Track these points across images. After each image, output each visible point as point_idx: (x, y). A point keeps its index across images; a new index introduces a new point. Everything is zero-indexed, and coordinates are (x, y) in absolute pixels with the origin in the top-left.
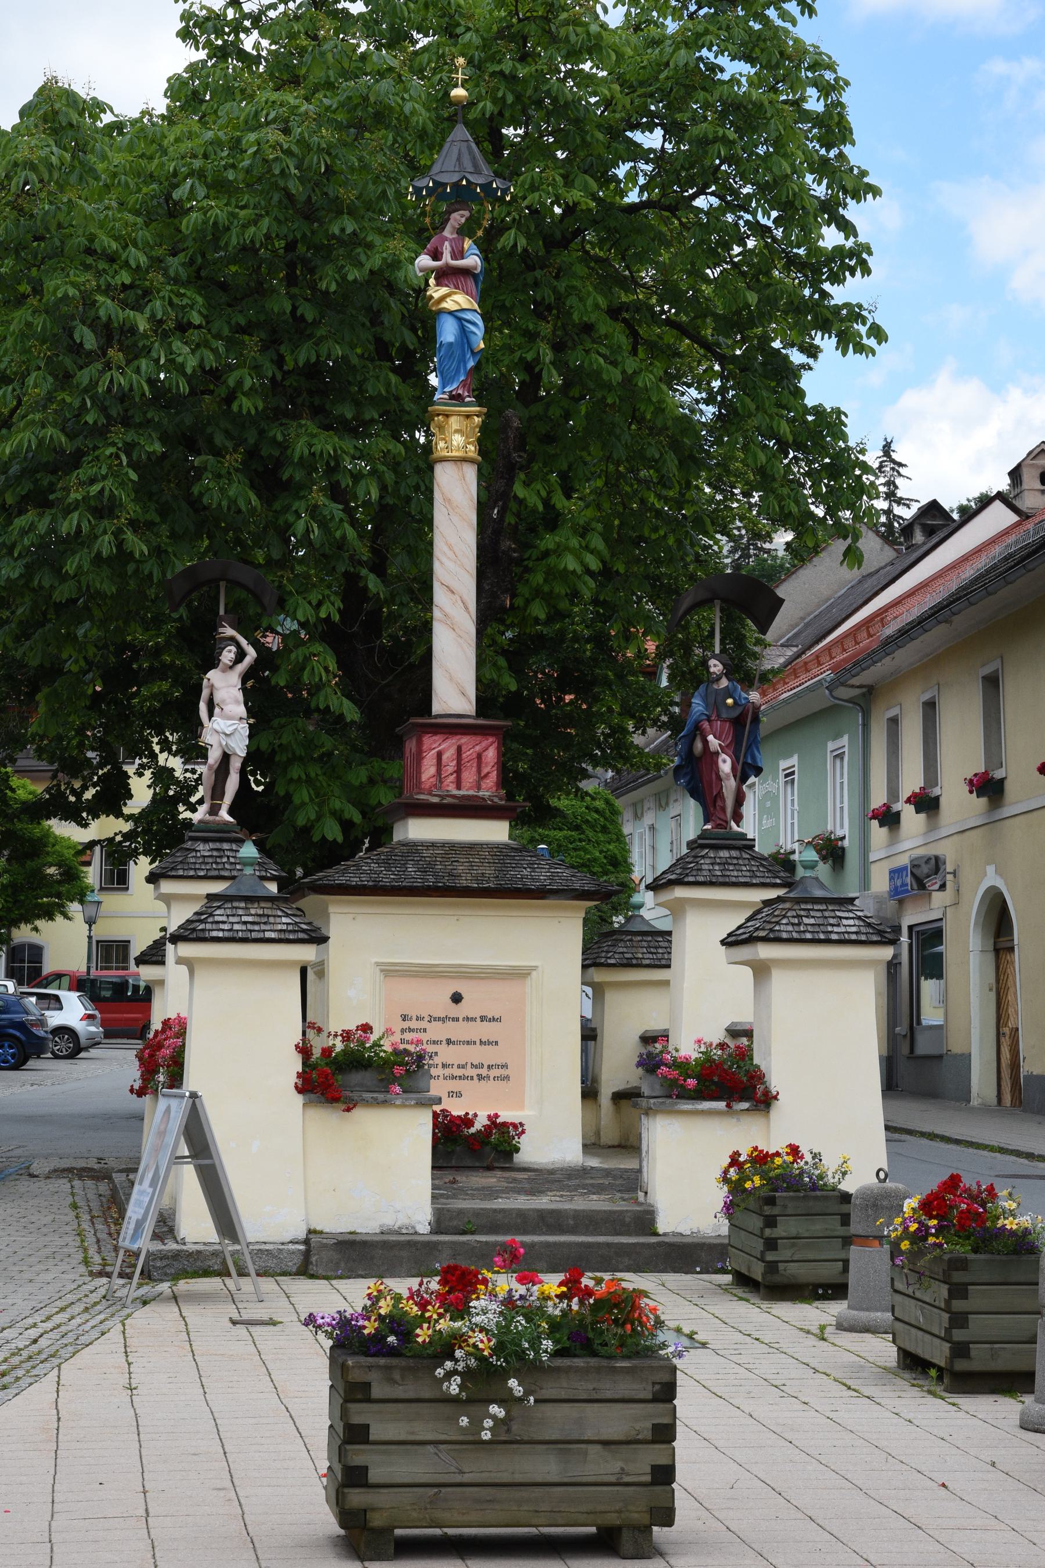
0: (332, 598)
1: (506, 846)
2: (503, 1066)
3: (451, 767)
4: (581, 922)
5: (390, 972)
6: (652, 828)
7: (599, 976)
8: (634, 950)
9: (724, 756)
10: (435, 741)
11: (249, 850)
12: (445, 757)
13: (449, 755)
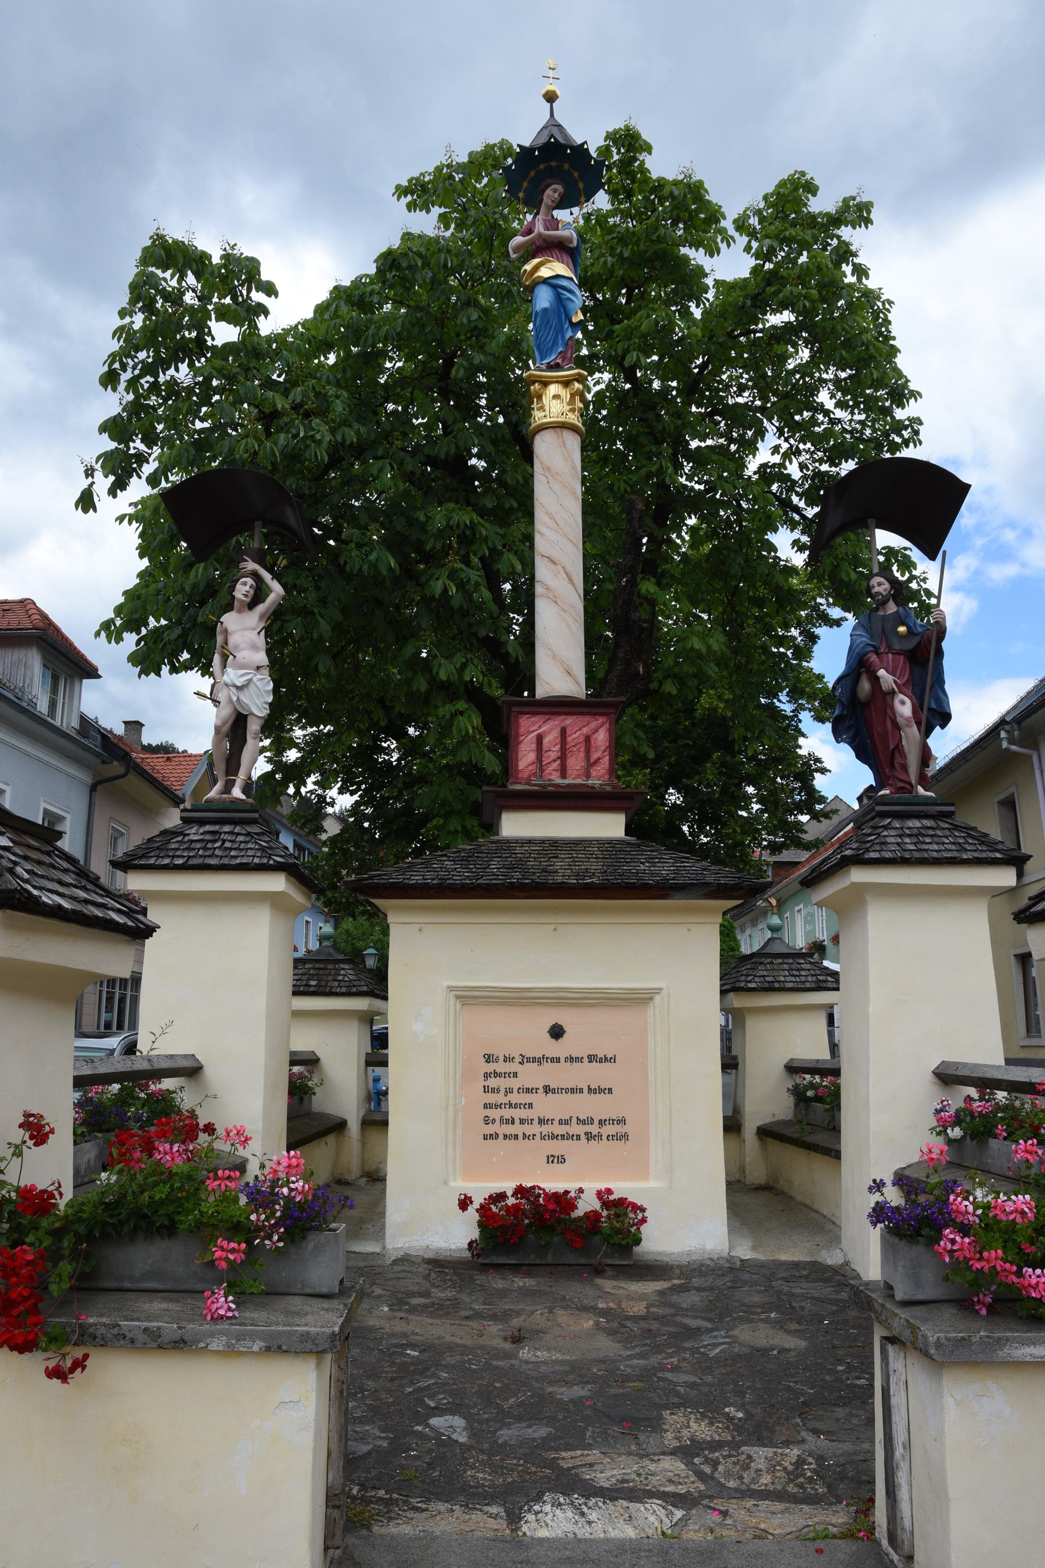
0: (475, 662)
1: (620, 841)
2: (619, 1122)
3: (554, 753)
4: (717, 929)
5: (469, 998)
6: (750, 936)
7: (738, 1001)
8: (775, 973)
9: (902, 696)
10: (534, 723)
11: (115, 763)
12: (546, 741)
13: (551, 738)
